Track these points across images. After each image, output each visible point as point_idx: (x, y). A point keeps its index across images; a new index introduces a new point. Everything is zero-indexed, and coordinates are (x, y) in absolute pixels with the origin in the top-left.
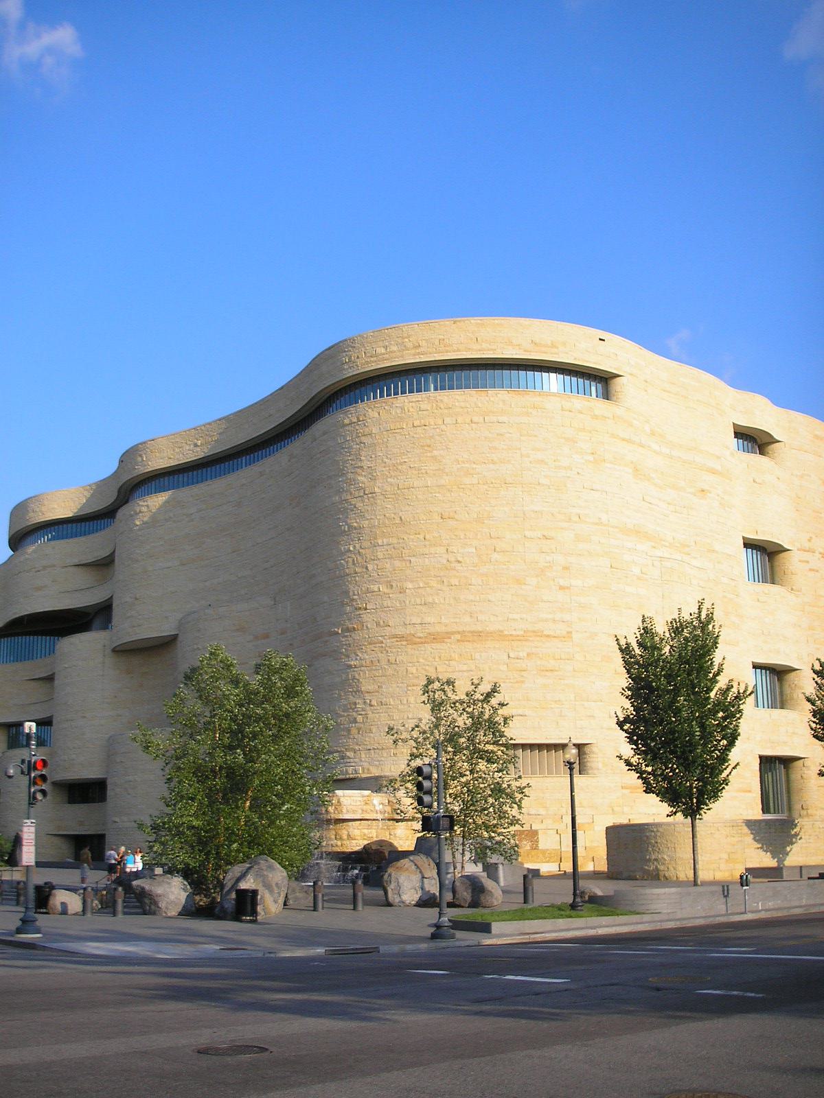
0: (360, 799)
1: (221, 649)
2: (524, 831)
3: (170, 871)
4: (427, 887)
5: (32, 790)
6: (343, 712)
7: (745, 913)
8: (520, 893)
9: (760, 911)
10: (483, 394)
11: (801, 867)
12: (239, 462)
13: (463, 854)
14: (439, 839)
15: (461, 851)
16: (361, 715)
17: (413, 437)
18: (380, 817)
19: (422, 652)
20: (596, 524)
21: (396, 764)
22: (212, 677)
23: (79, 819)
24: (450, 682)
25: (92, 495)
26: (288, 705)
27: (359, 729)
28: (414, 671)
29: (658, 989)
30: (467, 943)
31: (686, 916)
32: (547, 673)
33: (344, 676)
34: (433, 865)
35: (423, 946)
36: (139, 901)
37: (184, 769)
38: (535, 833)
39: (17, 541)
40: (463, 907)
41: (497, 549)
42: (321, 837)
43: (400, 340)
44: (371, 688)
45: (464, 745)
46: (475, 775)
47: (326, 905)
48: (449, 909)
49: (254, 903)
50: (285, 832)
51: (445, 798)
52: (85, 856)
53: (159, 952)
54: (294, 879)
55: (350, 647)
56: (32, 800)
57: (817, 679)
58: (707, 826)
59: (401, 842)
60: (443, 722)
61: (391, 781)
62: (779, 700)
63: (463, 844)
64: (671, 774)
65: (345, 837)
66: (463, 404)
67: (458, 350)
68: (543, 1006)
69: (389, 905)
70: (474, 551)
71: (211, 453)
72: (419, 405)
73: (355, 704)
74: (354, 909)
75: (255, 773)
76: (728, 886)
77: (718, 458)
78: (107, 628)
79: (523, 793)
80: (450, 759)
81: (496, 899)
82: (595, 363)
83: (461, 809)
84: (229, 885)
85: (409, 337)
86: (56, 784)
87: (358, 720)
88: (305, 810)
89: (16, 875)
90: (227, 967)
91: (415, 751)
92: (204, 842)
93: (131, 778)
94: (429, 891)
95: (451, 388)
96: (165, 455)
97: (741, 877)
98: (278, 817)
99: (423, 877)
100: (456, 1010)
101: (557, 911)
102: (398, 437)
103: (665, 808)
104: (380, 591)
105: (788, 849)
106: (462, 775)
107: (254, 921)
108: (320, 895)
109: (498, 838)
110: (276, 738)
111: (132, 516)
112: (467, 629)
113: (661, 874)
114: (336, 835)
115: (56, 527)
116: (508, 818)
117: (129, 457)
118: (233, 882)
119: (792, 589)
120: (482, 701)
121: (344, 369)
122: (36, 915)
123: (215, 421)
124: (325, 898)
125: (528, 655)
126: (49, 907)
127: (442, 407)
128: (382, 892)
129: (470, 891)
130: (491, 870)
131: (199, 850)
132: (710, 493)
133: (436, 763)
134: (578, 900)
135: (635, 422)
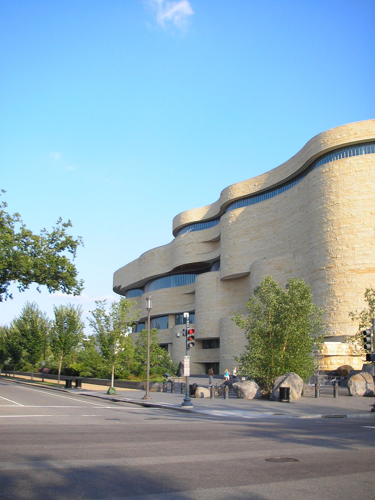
3: (249, 379)
4: (369, 388)
5: (188, 343)
16: (336, 307)
21: (354, 329)
22: (267, 291)
23: (208, 356)
25: (209, 210)
27: (335, 314)
28: (360, 286)
35: (368, 415)
39: (177, 232)
43: (347, 132)
44: (340, 294)
49: (288, 394)
53: (245, 415)
56: (188, 347)
59: (356, 366)
65: (329, 363)
69: (351, 395)
74: (334, 397)
78: (218, 270)
84: (276, 384)
85: (351, 129)
86: (198, 340)
87: (334, 309)
91: (361, 324)
92: (264, 366)
93: (230, 337)
94: (370, 389)
99: (367, 383)
102: (349, 177)
107: (288, 402)
111: (227, 219)
117: (224, 192)
121: (322, 147)
122: (190, 398)
124: (321, 392)
126: (195, 395)
131: (262, 369)
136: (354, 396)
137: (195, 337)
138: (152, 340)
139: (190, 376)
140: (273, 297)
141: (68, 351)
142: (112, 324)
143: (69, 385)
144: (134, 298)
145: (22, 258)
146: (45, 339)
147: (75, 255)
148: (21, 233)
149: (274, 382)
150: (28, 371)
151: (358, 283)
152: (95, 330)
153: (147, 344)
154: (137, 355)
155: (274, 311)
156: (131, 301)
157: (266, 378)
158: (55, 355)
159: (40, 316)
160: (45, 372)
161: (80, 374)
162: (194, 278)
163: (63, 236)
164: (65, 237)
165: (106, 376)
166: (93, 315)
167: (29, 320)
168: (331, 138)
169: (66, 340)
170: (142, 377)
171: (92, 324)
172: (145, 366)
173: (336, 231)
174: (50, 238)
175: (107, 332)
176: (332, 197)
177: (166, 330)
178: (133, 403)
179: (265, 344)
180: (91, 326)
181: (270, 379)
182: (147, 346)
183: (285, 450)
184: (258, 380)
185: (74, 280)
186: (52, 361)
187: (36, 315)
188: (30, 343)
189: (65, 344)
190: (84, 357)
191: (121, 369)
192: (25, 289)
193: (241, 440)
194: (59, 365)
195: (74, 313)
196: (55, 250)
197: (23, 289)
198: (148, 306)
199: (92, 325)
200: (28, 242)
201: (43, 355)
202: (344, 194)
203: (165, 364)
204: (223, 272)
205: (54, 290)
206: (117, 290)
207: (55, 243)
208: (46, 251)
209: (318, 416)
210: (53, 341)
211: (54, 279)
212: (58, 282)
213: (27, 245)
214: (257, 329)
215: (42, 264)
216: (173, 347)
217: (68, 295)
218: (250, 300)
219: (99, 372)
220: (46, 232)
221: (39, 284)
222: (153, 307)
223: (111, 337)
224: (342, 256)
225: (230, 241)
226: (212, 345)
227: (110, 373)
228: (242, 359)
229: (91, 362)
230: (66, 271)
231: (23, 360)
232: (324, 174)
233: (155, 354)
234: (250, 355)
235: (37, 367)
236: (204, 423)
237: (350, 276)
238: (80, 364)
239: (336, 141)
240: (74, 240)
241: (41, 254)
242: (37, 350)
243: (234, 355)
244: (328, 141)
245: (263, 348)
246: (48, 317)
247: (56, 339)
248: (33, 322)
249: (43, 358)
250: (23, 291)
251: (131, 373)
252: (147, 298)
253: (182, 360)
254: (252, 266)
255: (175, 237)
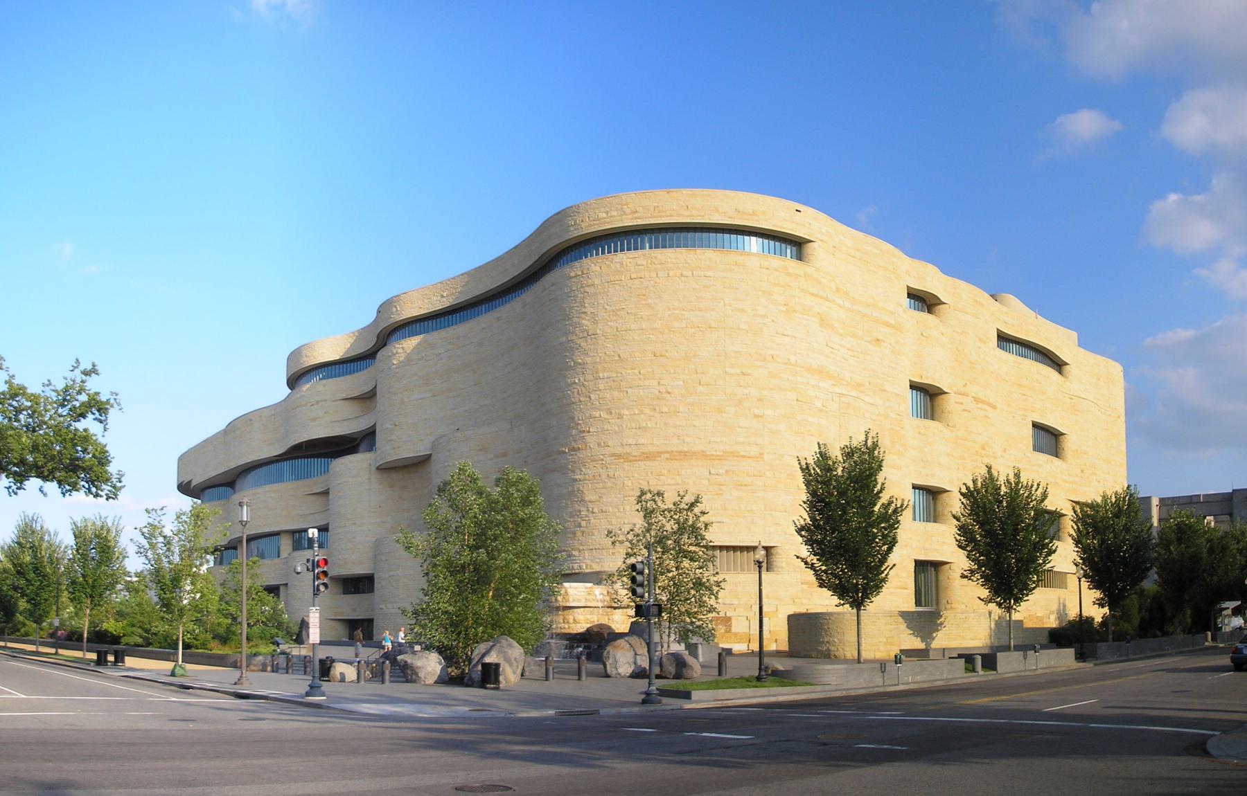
0: (584, 590)
1: (469, 465)
2: (719, 617)
3: (428, 648)
4: (639, 662)
5: (316, 583)
6: (570, 518)
7: (898, 685)
8: (716, 667)
9: (910, 683)
10: (692, 252)
11: (944, 649)
12: (480, 310)
13: (669, 636)
14: (649, 623)
15: (667, 633)
17: (630, 288)
18: (600, 605)
19: (637, 469)
20: (786, 364)
21: (614, 561)
22: (462, 490)
23: (353, 606)
24: (659, 494)
25: (355, 341)
26: (524, 512)
27: (583, 532)
28: (630, 484)
29: (825, 744)
30: (671, 707)
31: (849, 687)
32: (743, 488)
33: (570, 488)
34: (644, 644)
35: (636, 710)
36: (403, 672)
37: (440, 565)
38: (730, 619)
39: (294, 381)
40: (668, 678)
41: (702, 383)
42: (552, 621)
43: (619, 207)
44: (593, 498)
45: (671, 546)
46: (680, 571)
47: (556, 676)
48: (657, 680)
49: (497, 674)
50: (522, 617)
51: (655, 590)
52: (358, 637)
53: (420, 712)
54: (529, 654)
55: (575, 463)
56: (316, 591)
57: (963, 500)
58: (870, 616)
59: (618, 626)
60: (654, 527)
61: (610, 575)
62: (932, 515)
63: (669, 628)
64: (841, 573)
65: (571, 621)
66: (674, 261)
67: (671, 216)
68: (732, 757)
69: (608, 676)
70: (682, 384)
71: (456, 302)
72: (635, 261)
73: (580, 511)
74: (579, 679)
75: (496, 569)
76: (885, 664)
77: (893, 313)
78: (372, 450)
79: (719, 586)
80: (659, 558)
81: (696, 672)
82: (791, 230)
83: (668, 599)
84: (476, 658)
85: (627, 204)
86: (335, 579)
87: (582, 524)
88: (538, 599)
89: (303, 651)
90: (476, 724)
91: (630, 550)
92: (455, 624)
93: (394, 573)
94: (640, 666)
95: (664, 247)
96: (416, 305)
97: (896, 656)
98: (516, 604)
99: (636, 654)
100: (662, 760)
101: (745, 682)
102: (617, 287)
103: (836, 600)
104: (601, 417)
105: (934, 635)
106: (669, 571)
107: (497, 689)
108: (551, 668)
109: (698, 623)
110: (513, 540)
111: (390, 356)
112: (675, 449)
113: (832, 653)
114: (564, 620)
115: (326, 368)
116: (707, 607)
117: (385, 308)
118: (479, 656)
119: (948, 425)
120: (687, 510)
121: (570, 231)
122: (322, 683)
123: (458, 276)
124: (555, 671)
125: (726, 471)
126: (330, 676)
127: (656, 262)
128: (602, 666)
129: (674, 665)
130: (692, 649)
131: (451, 631)
132: (884, 342)
133: (648, 561)
134: (763, 673)
135: (823, 280)
136: (613, 677)
137: (329, 573)
138: (251, 578)
139: (320, 644)
140: (472, 500)
141: (100, 599)
142: (177, 550)
143: (103, 661)
144: (217, 503)
145: (11, 436)
146: (58, 579)
147: (107, 426)
148: (7, 390)
149: (472, 653)
150: (29, 635)
151: (626, 479)
152: (147, 562)
153: (242, 587)
154: (224, 606)
155: (475, 526)
156: (209, 508)
157: (457, 646)
158: (75, 607)
159: (46, 538)
160: (60, 637)
161: (122, 641)
162: (326, 465)
163: (83, 393)
164: (88, 394)
165: (169, 644)
166: (143, 534)
167: (28, 546)
168: (589, 217)
169: (95, 580)
170: (233, 646)
171: (141, 552)
172: (239, 626)
173: (590, 385)
174: (60, 398)
175: (167, 565)
176: (584, 322)
177: (277, 560)
178: (218, 691)
179: (457, 586)
180: (139, 555)
181: (465, 647)
182: (241, 590)
183: (490, 771)
184: (443, 649)
185: (106, 472)
186: (71, 618)
187: (39, 536)
188: (31, 587)
189: (93, 587)
190: (129, 610)
191: (194, 631)
192: (18, 491)
193: (412, 755)
194: (85, 625)
195: (108, 531)
196: (69, 419)
197: (15, 490)
198: (242, 517)
199: (141, 553)
200: (20, 406)
201: (54, 608)
202: (608, 318)
203: (275, 621)
204: (381, 453)
205: (70, 491)
206: (184, 488)
207: (69, 407)
208: (53, 422)
209: (549, 712)
210: (71, 583)
211: (70, 471)
212: (77, 476)
213: (18, 411)
214: (443, 558)
215: (46, 445)
216: (289, 592)
217: (95, 499)
218: (430, 505)
219: (155, 638)
220: (52, 387)
221: (43, 480)
222: (251, 518)
223: (176, 574)
224: (599, 430)
225: (394, 398)
226: (361, 587)
227: (175, 638)
228: (416, 613)
229: (141, 619)
230: (90, 456)
231: (20, 617)
232: (573, 280)
233: (256, 605)
234: (429, 606)
235: (45, 628)
236: (345, 726)
237: (612, 466)
238: (121, 623)
239: (598, 222)
240: (103, 398)
241: (45, 427)
242: (45, 599)
243: (400, 605)
244: (582, 221)
245: (453, 592)
246: (62, 540)
247: (78, 578)
248: (36, 548)
249: (55, 613)
250: (16, 494)
251: (213, 638)
252: (240, 503)
253: (305, 614)
254: (435, 443)
255: (291, 390)
